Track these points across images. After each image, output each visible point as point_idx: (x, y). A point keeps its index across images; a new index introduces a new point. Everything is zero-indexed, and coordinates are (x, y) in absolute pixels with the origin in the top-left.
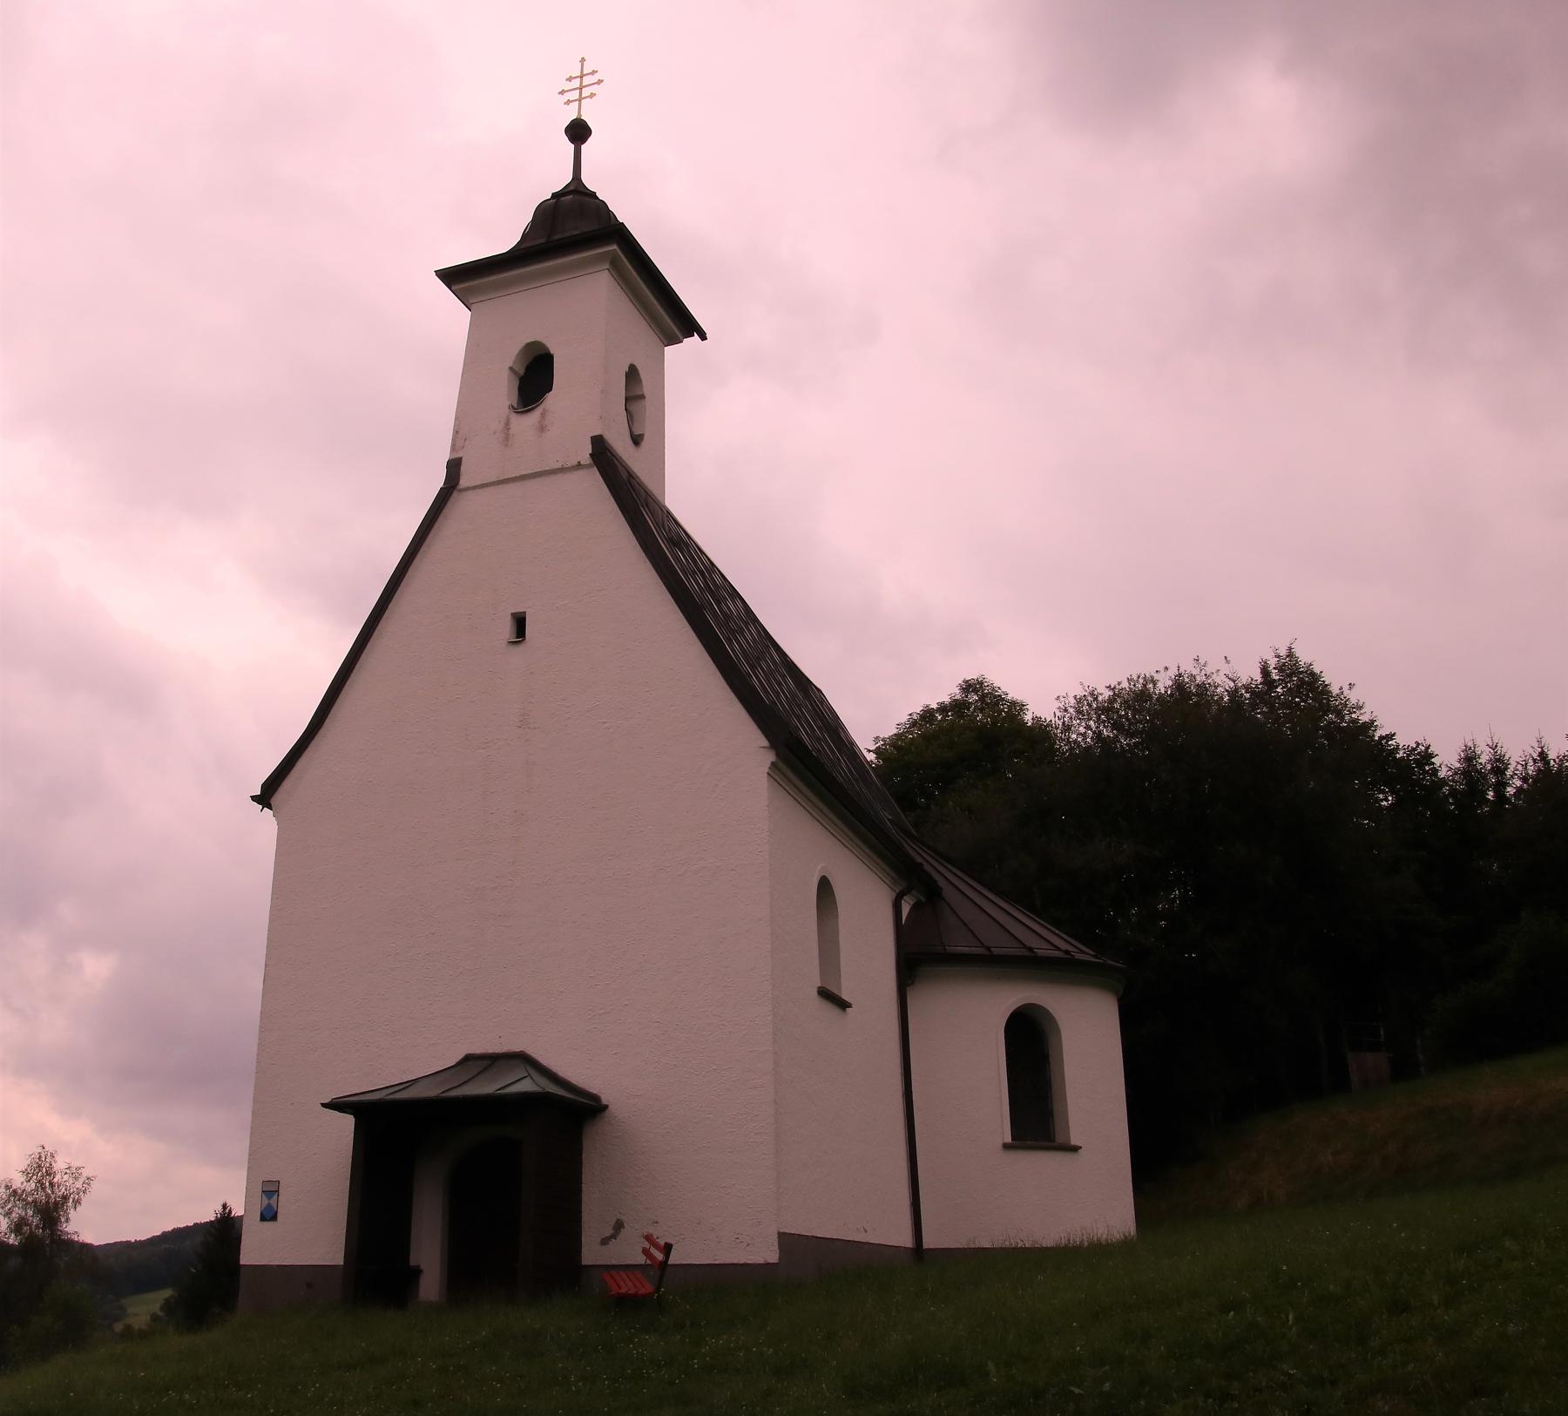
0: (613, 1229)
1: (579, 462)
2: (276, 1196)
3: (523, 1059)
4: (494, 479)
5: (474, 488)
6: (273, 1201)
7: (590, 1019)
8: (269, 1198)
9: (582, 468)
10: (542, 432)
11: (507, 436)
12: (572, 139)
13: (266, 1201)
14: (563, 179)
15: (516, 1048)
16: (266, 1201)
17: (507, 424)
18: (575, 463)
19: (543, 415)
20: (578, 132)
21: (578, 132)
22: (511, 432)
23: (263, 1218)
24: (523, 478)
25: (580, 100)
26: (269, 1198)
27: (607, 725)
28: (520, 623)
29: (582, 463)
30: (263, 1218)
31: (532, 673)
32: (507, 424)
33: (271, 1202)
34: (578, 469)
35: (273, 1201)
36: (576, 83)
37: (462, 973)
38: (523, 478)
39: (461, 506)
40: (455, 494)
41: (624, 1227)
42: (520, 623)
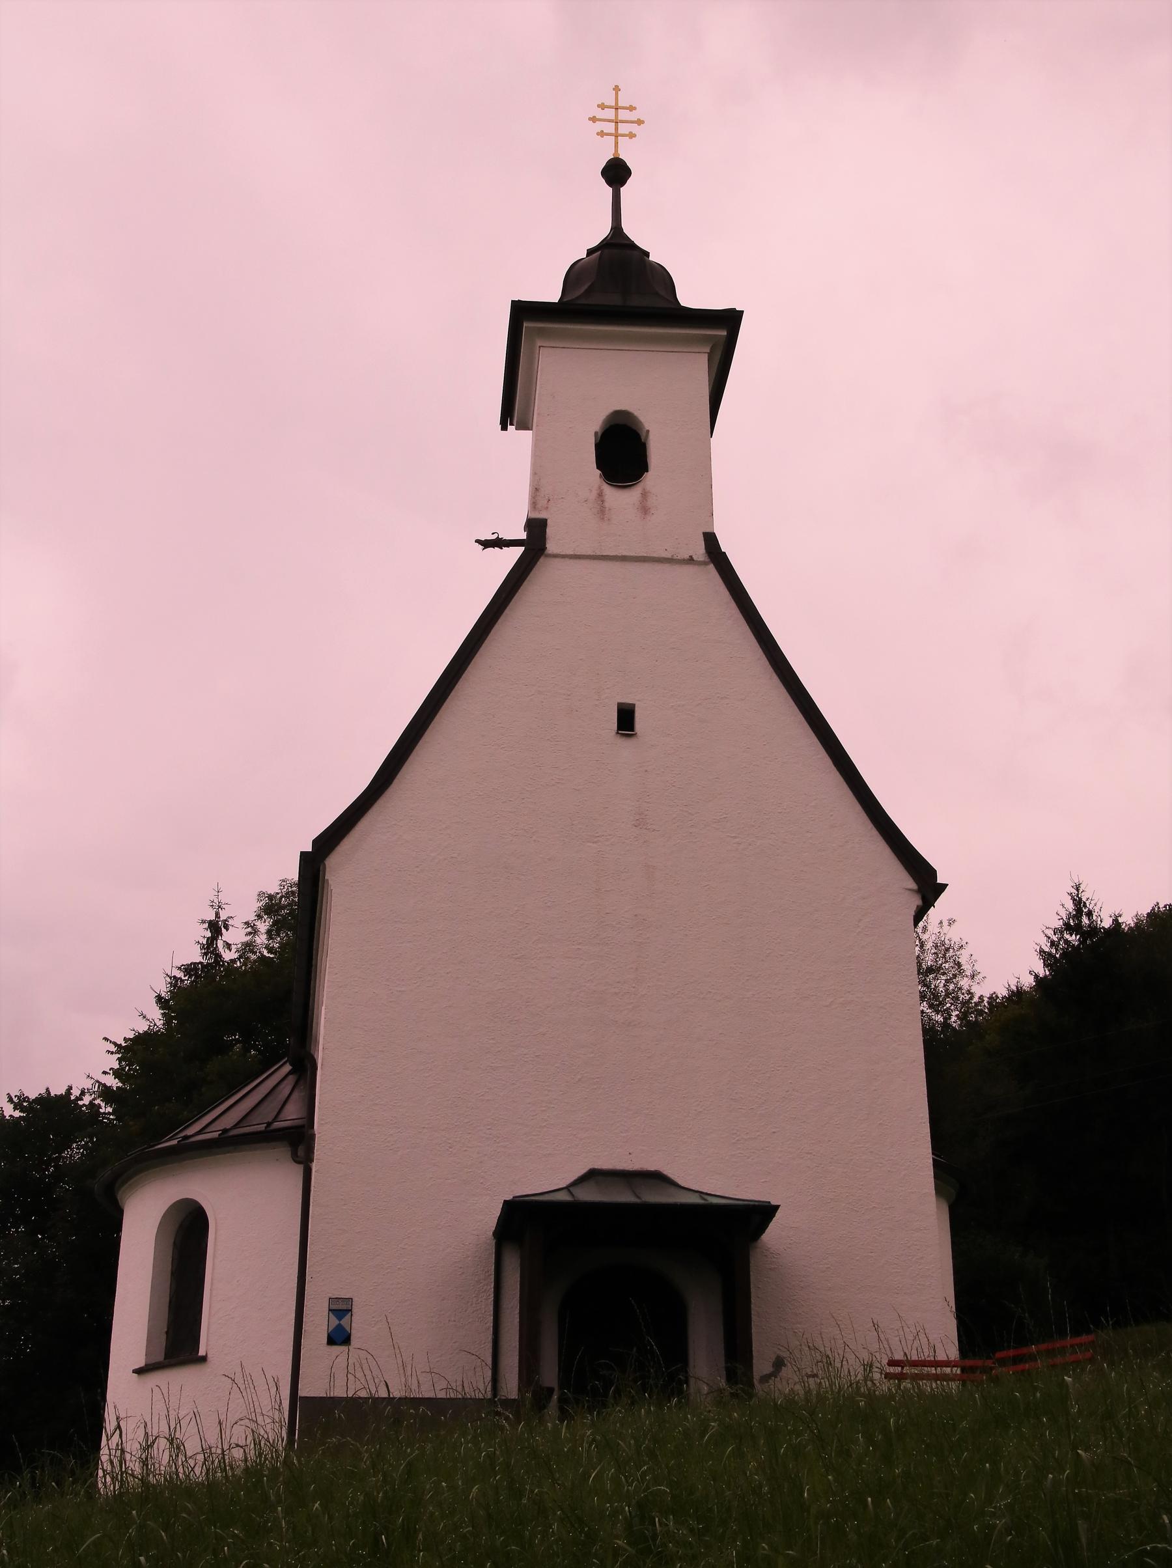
0: (773, 1366)
1: (691, 557)
2: (350, 1314)
3: (657, 1178)
4: (590, 553)
5: (564, 556)
6: (345, 1322)
7: (734, 1143)
8: (340, 1318)
9: (695, 564)
10: (646, 514)
11: (602, 511)
12: (610, 182)
13: (335, 1322)
14: (601, 231)
15: (652, 1167)
16: (335, 1322)
17: (600, 494)
18: (687, 557)
19: (645, 495)
20: (616, 173)
21: (616, 173)
22: (607, 505)
23: (331, 1341)
24: (624, 559)
25: (617, 136)
26: (340, 1318)
27: (737, 840)
28: (626, 719)
29: (695, 558)
30: (331, 1341)
31: (646, 771)
32: (600, 494)
33: (337, 1322)
34: (688, 564)
35: (345, 1322)
36: (610, 114)
37: (580, 1080)
38: (624, 559)
39: (545, 574)
40: (542, 560)
41: (785, 1365)
42: (626, 719)
